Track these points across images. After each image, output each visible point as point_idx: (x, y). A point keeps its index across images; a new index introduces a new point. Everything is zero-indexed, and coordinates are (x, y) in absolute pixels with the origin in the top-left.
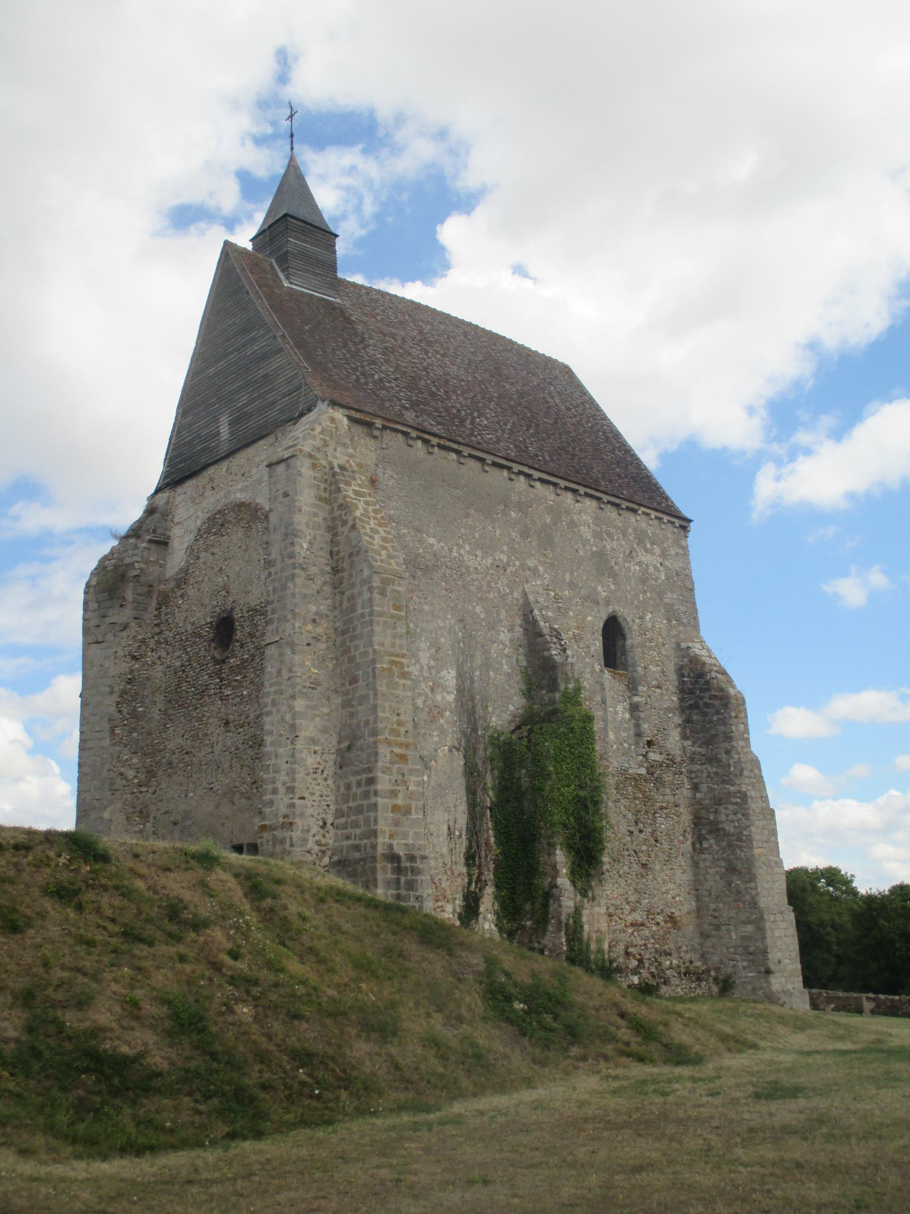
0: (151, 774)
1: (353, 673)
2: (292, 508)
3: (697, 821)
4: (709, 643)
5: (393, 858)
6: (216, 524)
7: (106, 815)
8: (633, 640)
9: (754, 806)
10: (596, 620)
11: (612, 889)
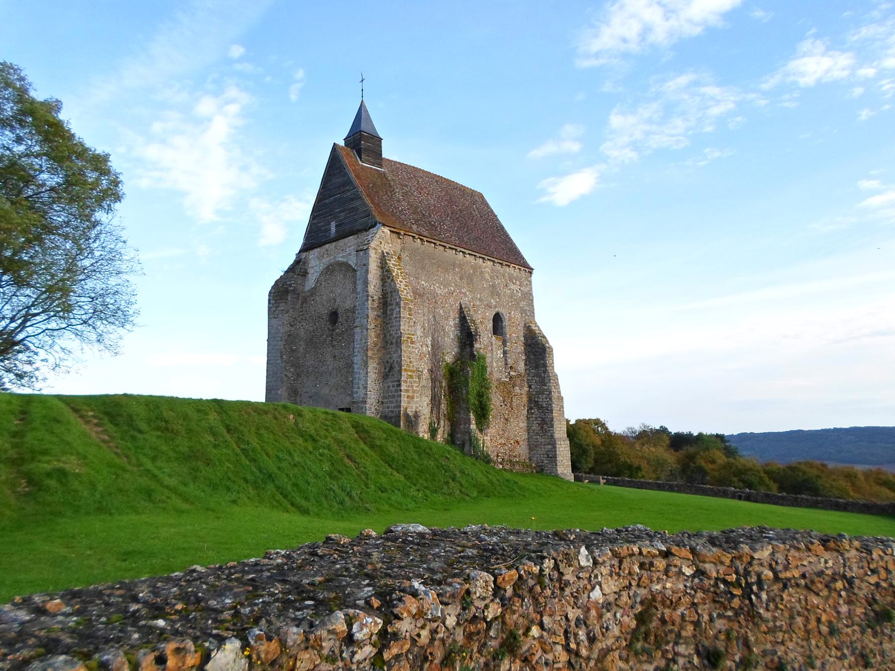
0: (298, 375)
1: (391, 341)
2: (367, 271)
3: (530, 400)
4: (539, 324)
5: (407, 416)
6: (329, 270)
7: (279, 392)
8: (506, 323)
9: (554, 395)
10: (490, 315)
11: (492, 431)
